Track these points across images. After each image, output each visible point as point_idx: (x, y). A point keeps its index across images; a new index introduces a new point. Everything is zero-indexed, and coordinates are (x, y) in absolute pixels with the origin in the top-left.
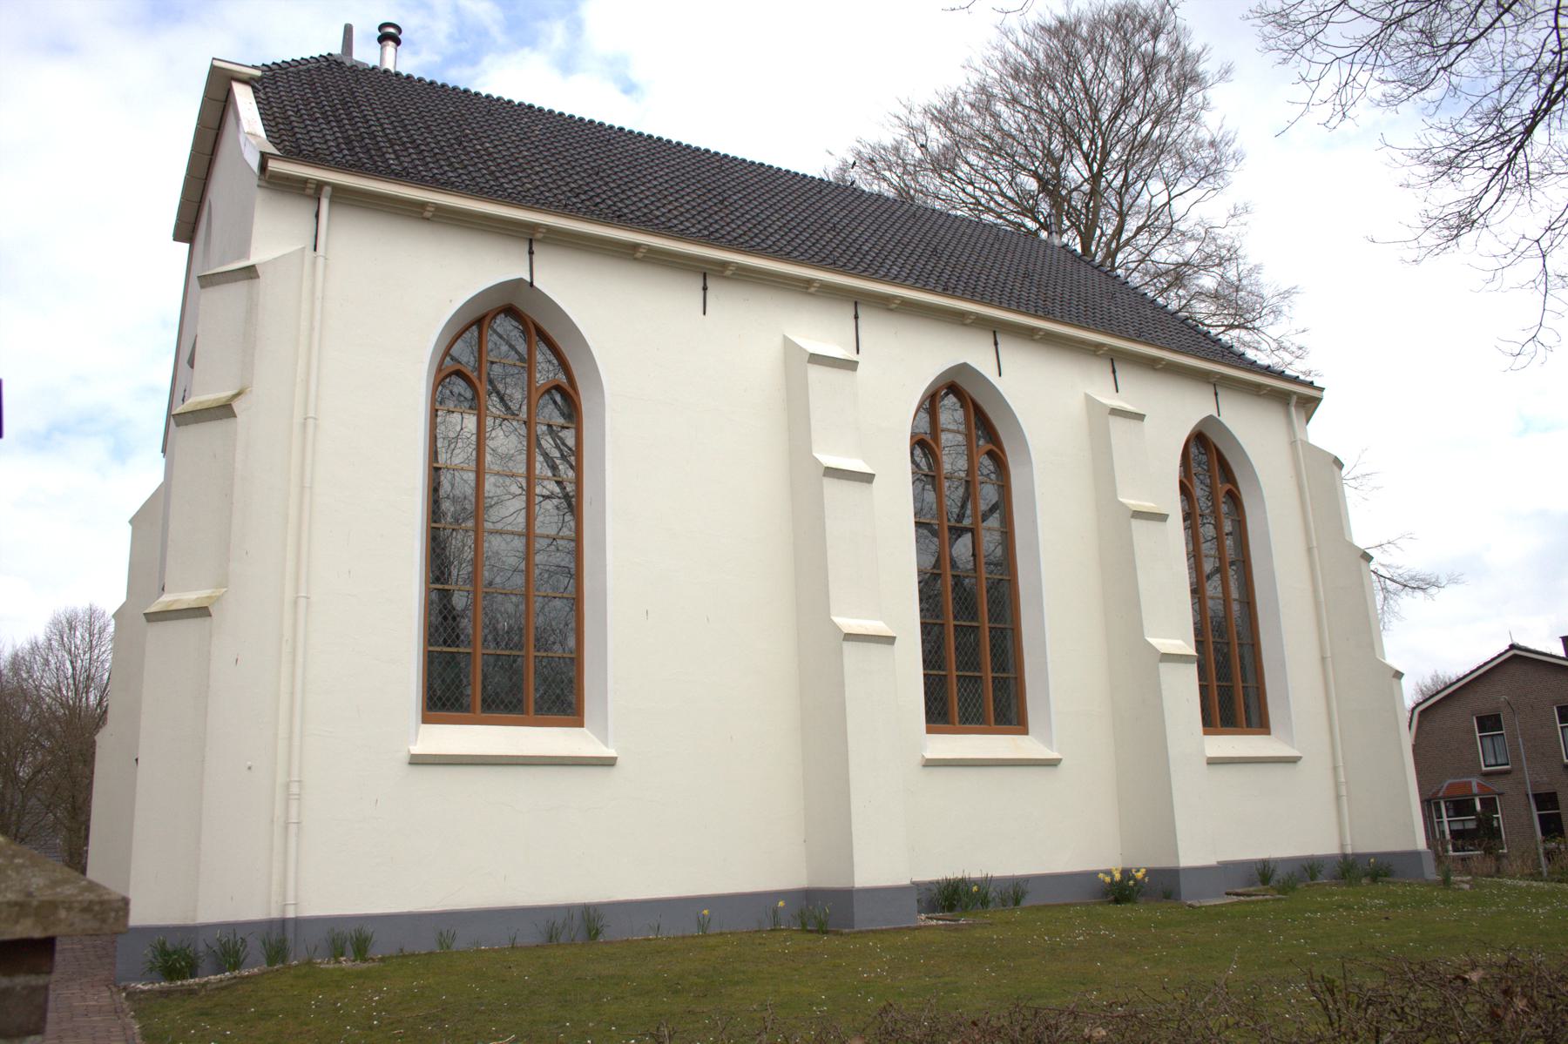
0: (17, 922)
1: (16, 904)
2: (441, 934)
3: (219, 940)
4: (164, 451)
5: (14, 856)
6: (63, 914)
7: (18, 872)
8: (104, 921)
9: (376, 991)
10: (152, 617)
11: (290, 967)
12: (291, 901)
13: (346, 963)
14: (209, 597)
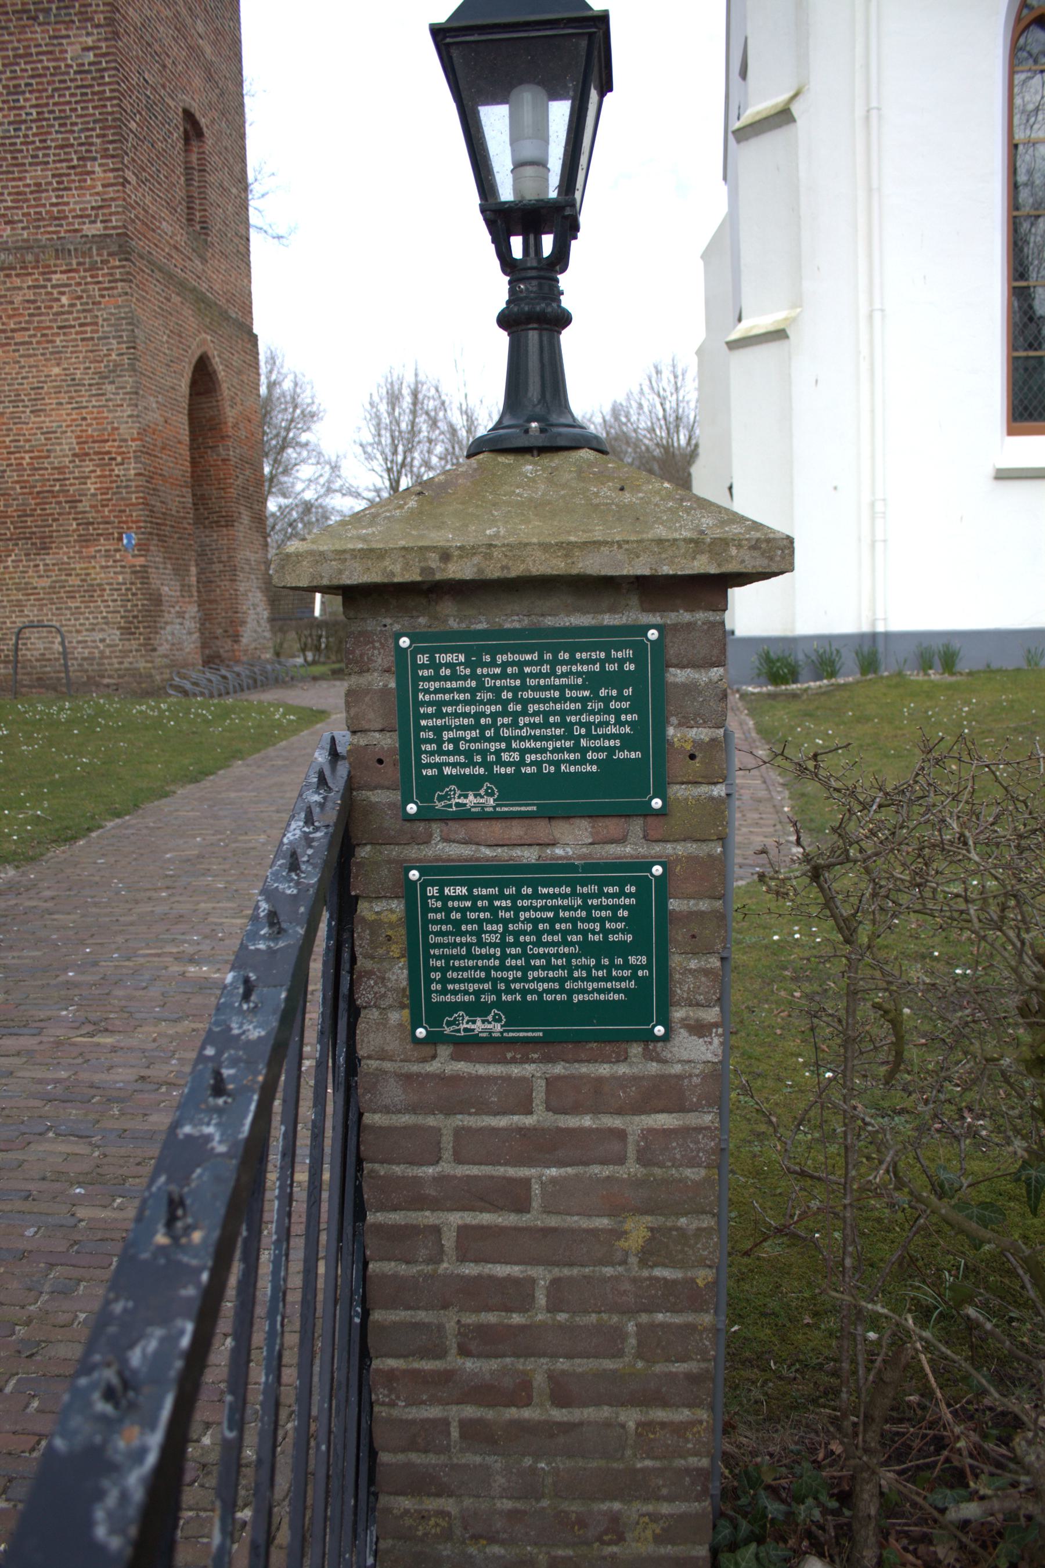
0: (694, 558)
1: (691, 540)
2: (1029, 651)
3: (816, 651)
4: (725, 178)
5: (682, 500)
6: (734, 551)
7: (688, 514)
8: (771, 559)
9: (126, 1384)
10: (734, 345)
11: (882, 678)
12: (880, 615)
13: (934, 675)
14: (786, 319)
